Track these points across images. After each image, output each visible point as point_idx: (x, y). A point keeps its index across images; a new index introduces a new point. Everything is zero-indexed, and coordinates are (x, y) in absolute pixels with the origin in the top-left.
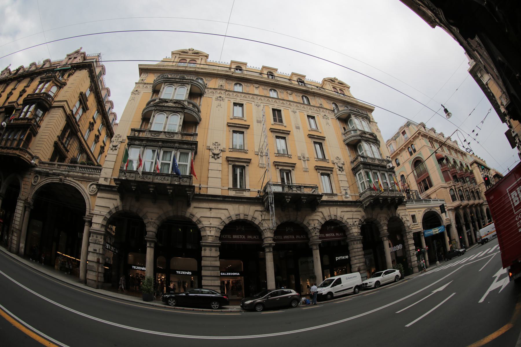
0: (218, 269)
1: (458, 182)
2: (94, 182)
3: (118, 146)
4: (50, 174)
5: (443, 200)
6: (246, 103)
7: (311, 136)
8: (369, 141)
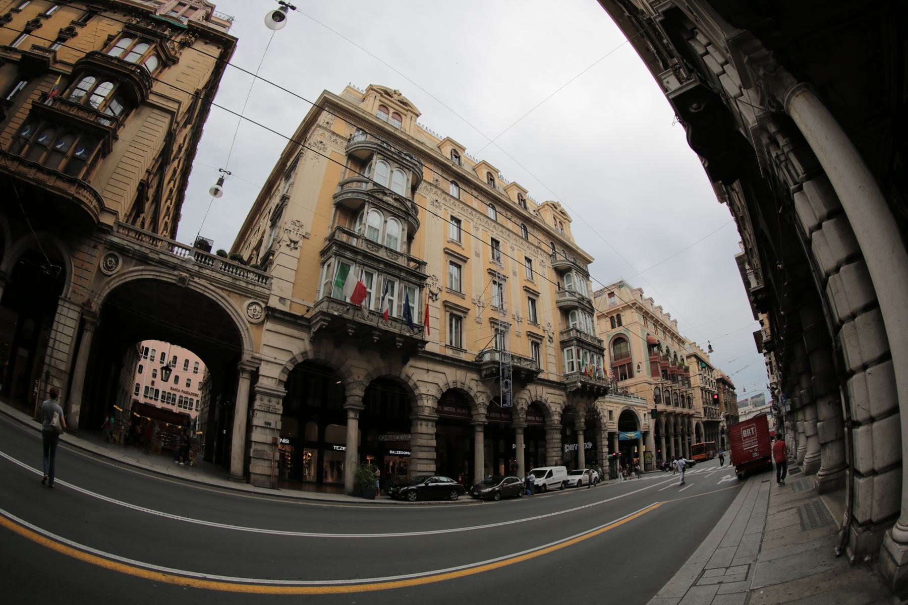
0: (433, 449)
1: (667, 379)
2: (256, 299)
3: (300, 244)
4: (152, 260)
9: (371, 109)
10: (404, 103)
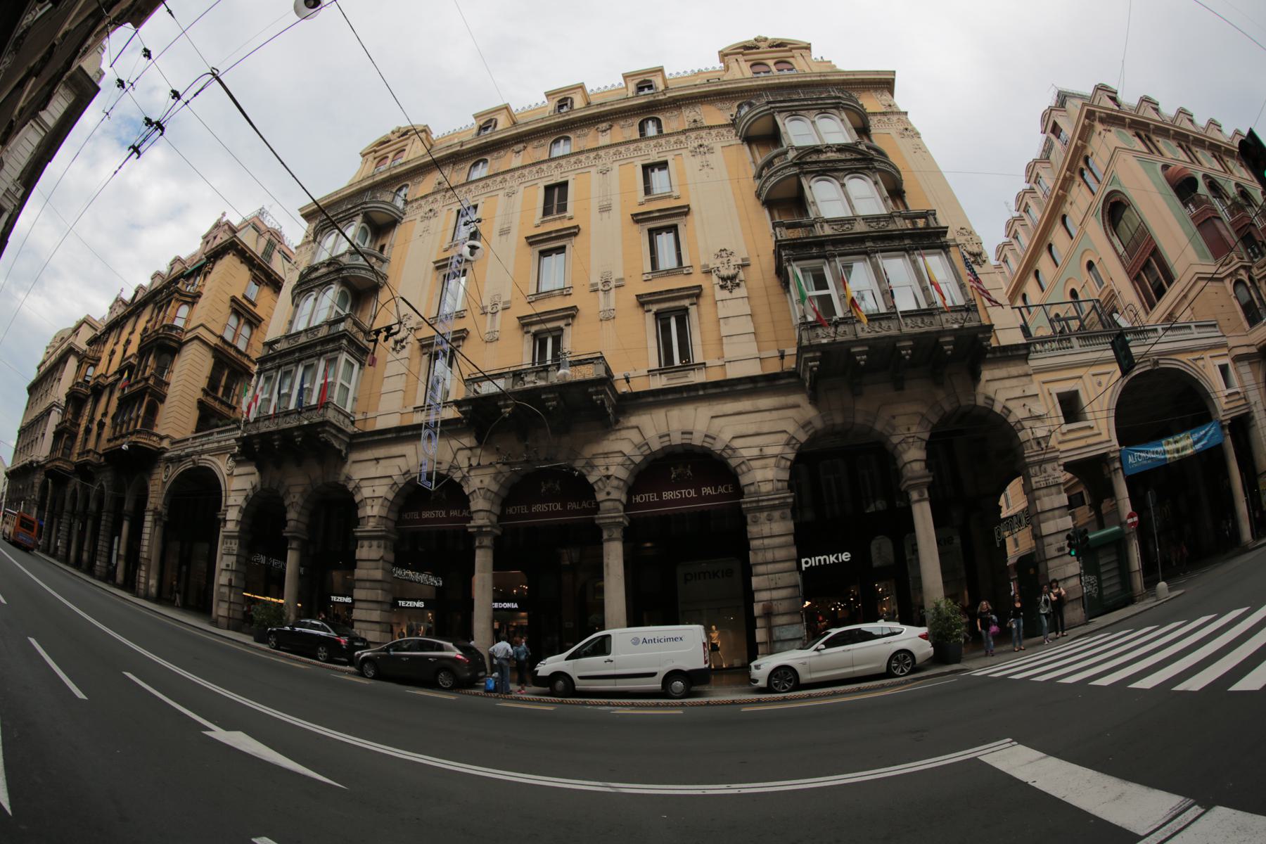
5: (1214, 326)
6: (673, 157)
7: (640, 217)
8: (837, 170)
9: (741, 73)
10: (781, 45)
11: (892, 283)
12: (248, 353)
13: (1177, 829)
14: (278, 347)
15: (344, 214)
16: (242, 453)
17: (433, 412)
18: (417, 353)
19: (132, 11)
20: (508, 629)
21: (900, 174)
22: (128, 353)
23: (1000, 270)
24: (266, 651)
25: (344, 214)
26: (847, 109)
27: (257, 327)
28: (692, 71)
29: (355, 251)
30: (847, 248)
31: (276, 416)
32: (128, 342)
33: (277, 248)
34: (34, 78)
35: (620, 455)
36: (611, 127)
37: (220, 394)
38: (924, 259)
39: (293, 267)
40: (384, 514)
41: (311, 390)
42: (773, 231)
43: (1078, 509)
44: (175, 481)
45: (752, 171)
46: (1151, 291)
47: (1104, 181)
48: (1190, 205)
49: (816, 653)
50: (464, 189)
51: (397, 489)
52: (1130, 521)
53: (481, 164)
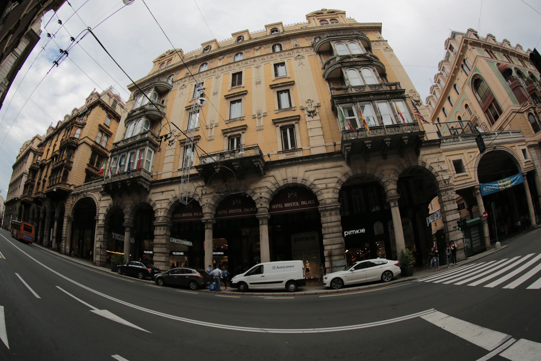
5: (520, 132)
7: (273, 86)
8: (357, 65)
9: (316, 24)
10: (332, 12)
11: (381, 113)
12: (106, 148)
13: (504, 348)
14: (119, 145)
15: (146, 88)
16: (104, 191)
17: (186, 171)
18: (179, 146)
19: (53, 5)
20: (219, 263)
21: (384, 67)
22: (55, 150)
23: (428, 108)
24: (117, 275)
25: (146, 88)
26: (362, 39)
27: (110, 137)
28: (295, 24)
29: (151, 103)
30: (362, 98)
31: (119, 174)
32: (55, 145)
33: (118, 103)
34: (12, 35)
35: (266, 188)
36: (260, 48)
37: (95, 166)
38: (395, 103)
39: (125, 111)
40: (166, 215)
41: (134, 163)
42: (330, 91)
43: (462, 210)
44: (76, 204)
45: (321, 66)
46: (493, 117)
47: (472, 70)
48: (509, 81)
49: (351, 272)
50: (198, 76)
51: (171, 205)
52: (484, 215)
53: (205, 65)
